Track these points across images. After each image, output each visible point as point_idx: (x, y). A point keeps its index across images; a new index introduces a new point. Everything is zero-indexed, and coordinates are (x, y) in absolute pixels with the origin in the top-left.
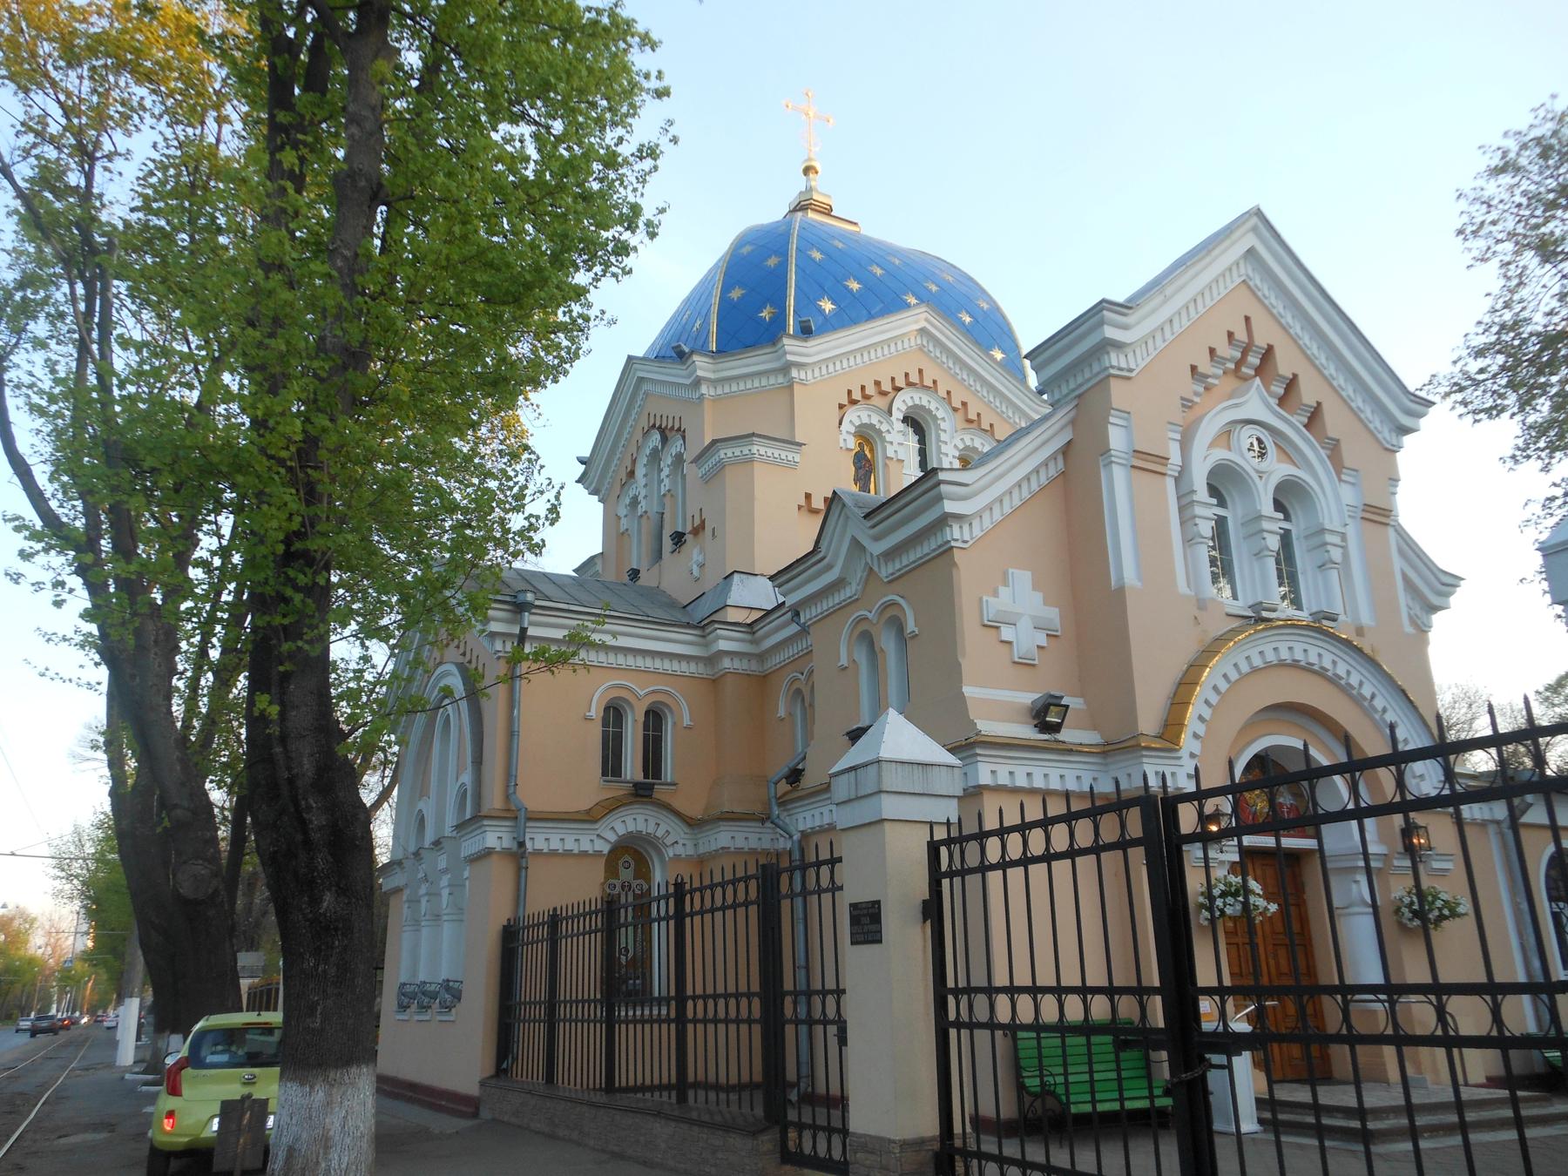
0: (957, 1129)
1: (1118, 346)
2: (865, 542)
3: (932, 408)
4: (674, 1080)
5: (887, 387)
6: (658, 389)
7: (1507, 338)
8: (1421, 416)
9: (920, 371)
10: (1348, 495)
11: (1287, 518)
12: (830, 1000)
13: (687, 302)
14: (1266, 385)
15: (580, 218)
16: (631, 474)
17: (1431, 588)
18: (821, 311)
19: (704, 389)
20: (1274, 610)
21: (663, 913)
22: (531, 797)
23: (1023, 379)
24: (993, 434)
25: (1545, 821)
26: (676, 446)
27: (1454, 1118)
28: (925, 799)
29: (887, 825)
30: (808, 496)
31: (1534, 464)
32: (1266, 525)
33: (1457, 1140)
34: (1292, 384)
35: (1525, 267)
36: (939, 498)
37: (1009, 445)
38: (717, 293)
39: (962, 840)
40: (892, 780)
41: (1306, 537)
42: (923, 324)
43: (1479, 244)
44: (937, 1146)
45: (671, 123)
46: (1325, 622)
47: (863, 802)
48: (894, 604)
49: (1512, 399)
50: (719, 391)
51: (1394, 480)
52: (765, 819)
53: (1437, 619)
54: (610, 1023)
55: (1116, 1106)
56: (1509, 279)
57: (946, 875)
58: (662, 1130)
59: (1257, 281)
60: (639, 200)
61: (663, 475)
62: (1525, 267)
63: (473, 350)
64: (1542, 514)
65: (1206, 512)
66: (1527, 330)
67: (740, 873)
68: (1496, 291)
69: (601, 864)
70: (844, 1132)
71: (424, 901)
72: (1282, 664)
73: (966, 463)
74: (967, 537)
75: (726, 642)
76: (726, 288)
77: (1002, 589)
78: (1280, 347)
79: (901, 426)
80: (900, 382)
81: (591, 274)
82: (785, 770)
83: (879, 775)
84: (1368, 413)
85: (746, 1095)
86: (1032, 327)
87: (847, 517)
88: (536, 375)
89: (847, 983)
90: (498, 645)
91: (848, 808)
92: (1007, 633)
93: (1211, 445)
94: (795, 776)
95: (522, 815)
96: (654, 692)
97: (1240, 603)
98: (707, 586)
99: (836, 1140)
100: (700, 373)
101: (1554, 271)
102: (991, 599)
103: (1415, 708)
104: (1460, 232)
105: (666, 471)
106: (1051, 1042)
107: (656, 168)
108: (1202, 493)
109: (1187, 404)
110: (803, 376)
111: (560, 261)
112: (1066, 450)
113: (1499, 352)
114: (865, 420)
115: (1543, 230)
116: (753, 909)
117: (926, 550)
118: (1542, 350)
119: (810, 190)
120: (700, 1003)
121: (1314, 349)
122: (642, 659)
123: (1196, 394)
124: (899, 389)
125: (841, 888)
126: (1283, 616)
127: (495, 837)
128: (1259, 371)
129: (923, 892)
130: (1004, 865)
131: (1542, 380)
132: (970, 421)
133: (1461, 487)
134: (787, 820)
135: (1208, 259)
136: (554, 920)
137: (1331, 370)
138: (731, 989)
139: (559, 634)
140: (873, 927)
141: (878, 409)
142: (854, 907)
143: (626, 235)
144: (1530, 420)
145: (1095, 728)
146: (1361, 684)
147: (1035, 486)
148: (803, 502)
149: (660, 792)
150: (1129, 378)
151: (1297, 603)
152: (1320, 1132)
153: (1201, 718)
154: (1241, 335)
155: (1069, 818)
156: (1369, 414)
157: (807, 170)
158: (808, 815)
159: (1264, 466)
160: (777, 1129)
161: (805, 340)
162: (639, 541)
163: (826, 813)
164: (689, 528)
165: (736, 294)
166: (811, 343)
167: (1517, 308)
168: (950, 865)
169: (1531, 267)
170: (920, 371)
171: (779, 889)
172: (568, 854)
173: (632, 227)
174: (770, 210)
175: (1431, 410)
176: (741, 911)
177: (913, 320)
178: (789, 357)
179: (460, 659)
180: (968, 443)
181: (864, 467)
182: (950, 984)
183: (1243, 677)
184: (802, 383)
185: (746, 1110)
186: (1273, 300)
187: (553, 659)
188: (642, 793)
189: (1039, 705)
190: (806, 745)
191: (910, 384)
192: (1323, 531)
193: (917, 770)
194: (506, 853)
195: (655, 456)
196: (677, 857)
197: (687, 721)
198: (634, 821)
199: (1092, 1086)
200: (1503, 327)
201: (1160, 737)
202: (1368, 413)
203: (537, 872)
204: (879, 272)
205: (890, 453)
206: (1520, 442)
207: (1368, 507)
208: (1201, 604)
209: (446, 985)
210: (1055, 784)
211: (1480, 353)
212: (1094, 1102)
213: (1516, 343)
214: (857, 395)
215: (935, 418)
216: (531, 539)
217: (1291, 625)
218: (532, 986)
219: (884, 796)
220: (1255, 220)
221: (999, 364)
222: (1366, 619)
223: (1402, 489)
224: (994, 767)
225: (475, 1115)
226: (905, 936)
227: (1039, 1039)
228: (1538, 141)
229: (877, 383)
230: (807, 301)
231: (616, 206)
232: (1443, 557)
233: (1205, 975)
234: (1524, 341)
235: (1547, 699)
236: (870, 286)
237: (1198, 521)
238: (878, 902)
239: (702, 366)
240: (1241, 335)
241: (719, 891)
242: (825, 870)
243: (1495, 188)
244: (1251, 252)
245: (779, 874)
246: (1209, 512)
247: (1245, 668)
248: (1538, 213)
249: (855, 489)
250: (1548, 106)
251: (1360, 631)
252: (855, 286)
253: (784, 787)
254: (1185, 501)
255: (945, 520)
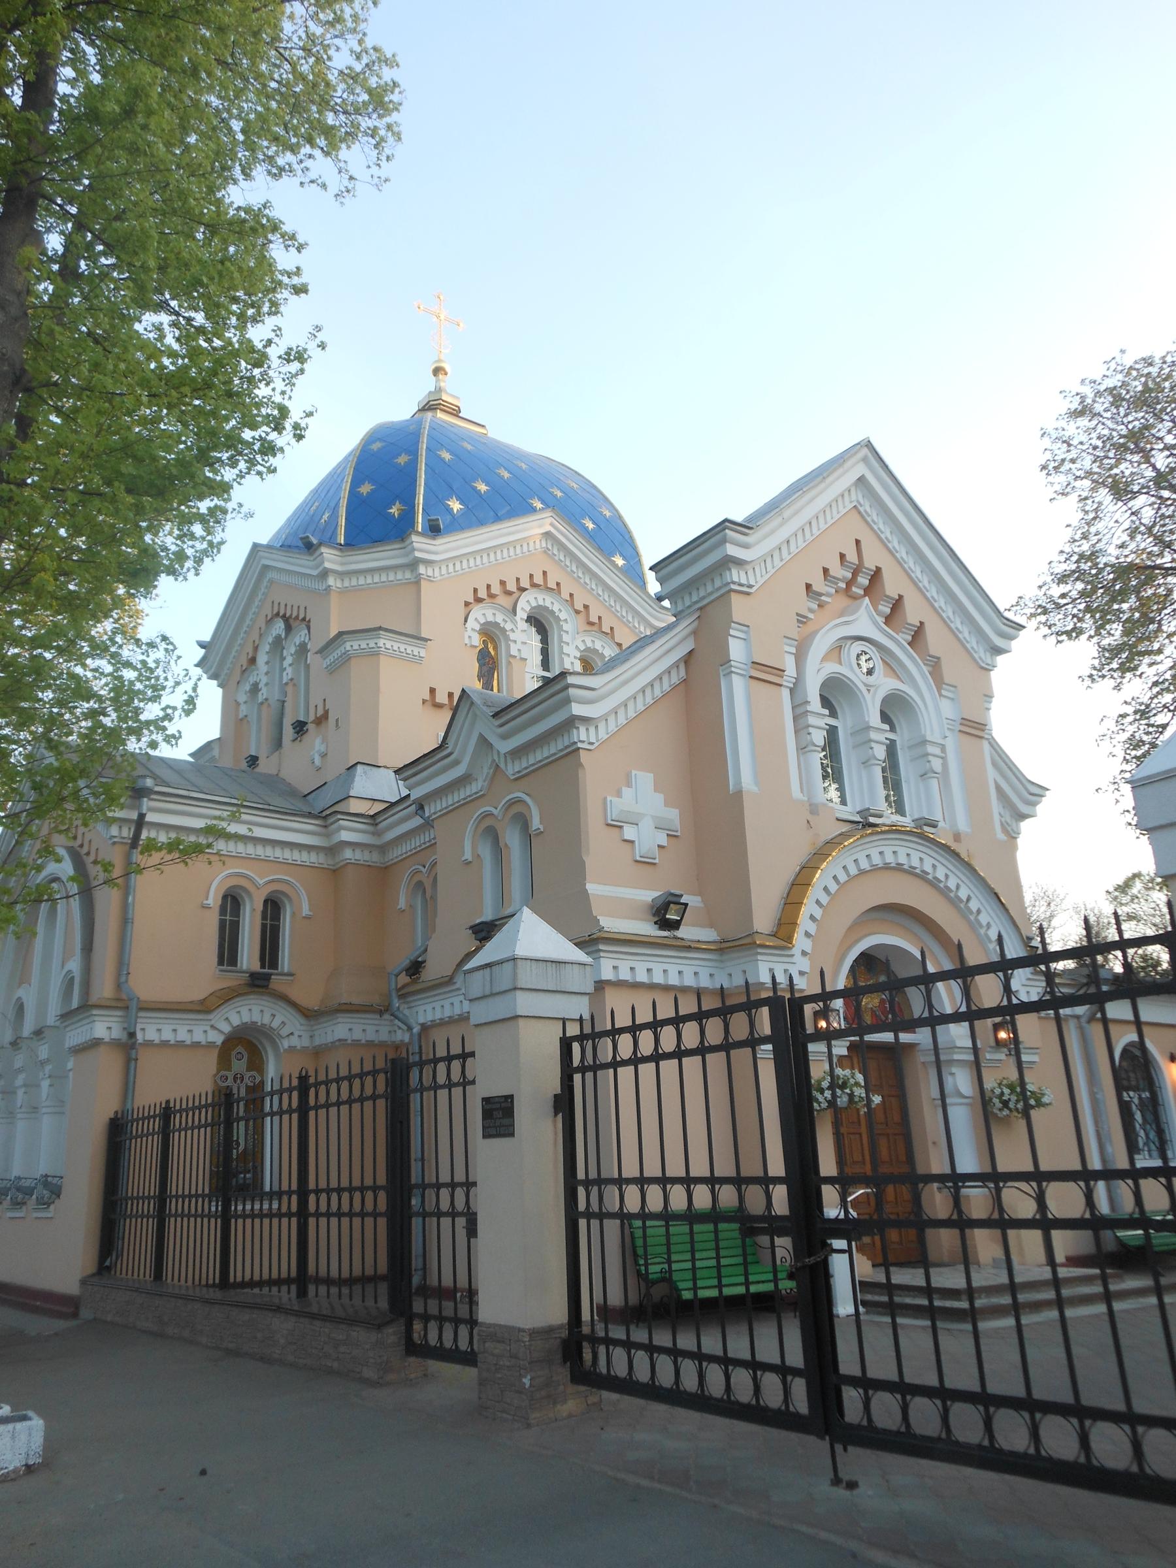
0: (586, 1315)
1: (740, 563)
2: (492, 739)
3: (555, 609)
4: (294, 1274)
5: (512, 586)
6: (284, 578)
7: (1085, 566)
8: (1012, 638)
9: (545, 573)
10: (947, 709)
11: (893, 729)
12: (460, 1193)
13: (315, 492)
14: (875, 605)
15: (220, 409)
16: (253, 661)
17: (1020, 797)
18: (449, 510)
19: (331, 581)
20: (880, 816)
21: (275, 1108)
22: (143, 987)
23: (643, 585)
24: (613, 638)
25: (1131, 1017)
26: (300, 636)
27: (1021, 1298)
28: (558, 996)
29: (521, 1022)
30: (432, 691)
31: (1109, 683)
32: (873, 735)
33: (1010, 1322)
34: (897, 604)
35: (1100, 503)
36: (567, 701)
37: (634, 653)
38: (346, 486)
39: (595, 1036)
40: (527, 976)
41: (910, 748)
42: (548, 528)
43: (1060, 479)
44: (565, 1334)
45: (318, 329)
46: (926, 828)
47: (498, 999)
48: (520, 801)
49: (1088, 623)
50: (346, 584)
51: (989, 696)
52: (384, 1010)
53: (1025, 825)
54: (226, 1218)
55: (741, 1290)
56: (1087, 512)
57: (577, 1070)
58: (282, 1326)
59: (866, 507)
60: (287, 403)
61: (286, 663)
62: (1100, 503)
63: (113, 540)
64: (1116, 729)
65: (819, 721)
66: (1102, 561)
67: (368, 1067)
68: (1075, 523)
69: (215, 1054)
70: (472, 1322)
71: (20, 1092)
72: (887, 867)
73: (588, 667)
74: (593, 740)
75: (349, 833)
76: (356, 483)
77: (624, 789)
78: (882, 563)
79: (525, 626)
80: (525, 583)
81: (236, 471)
82: (406, 963)
83: (515, 975)
84: (965, 633)
85: (357, 1289)
86: (658, 537)
87: (475, 715)
88: (176, 566)
89: (480, 1173)
90: (114, 831)
91: (482, 1004)
92: (629, 832)
93: (825, 659)
94: (415, 968)
95: (134, 1005)
96: (273, 881)
97: (849, 808)
98: (329, 775)
99: (463, 1331)
100: (327, 565)
101: (1125, 508)
102: (615, 800)
103: (1007, 910)
104: (1044, 467)
105: (289, 660)
106: (679, 1230)
107: (302, 371)
108: (815, 704)
109: (802, 620)
110: (430, 573)
111: (204, 458)
112: (688, 659)
113: (1077, 579)
114: (490, 618)
115: (1115, 471)
116: (381, 1103)
117: (553, 751)
118: (1115, 580)
119: (439, 390)
120: (323, 1196)
121: (917, 573)
122: (268, 848)
123: (811, 610)
124: (524, 590)
125: (473, 1082)
126: (888, 822)
127: (104, 1027)
128: (868, 591)
129: (554, 1085)
130: (636, 1061)
131: (1116, 607)
132: (591, 624)
133: (1056, 711)
134: (406, 1012)
135: (822, 486)
136: (167, 1113)
137: (933, 592)
138: (334, 1184)
139: (200, 824)
140: (506, 1121)
141: (502, 608)
142: (486, 1100)
143: (273, 436)
144: (1105, 642)
145: (711, 925)
146: (958, 887)
147: (658, 692)
148: (427, 697)
149: (277, 982)
150: (748, 594)
151: (900, 811)
152: (932, 1313)
153: (812, 918)
154: (852, 557)
155: (700, 1016)
156: (966, 634)
157: (437, 371)
158: (429, 1007)
159: (871, 680)
160: (402, 1321)
161: (434, 538)
162: (259, 730)
163: (438, 1009)
164: (312, 718)
165: (365, 489)
166: (439, 541)
167: (1094, 539)
168: (582, 1060)
169: (1105, 503)
170: (545, 573)
171: (400, 1082)
172: (180, 1045)
173: (279, 428)
174: (400, 409)
175: (1022, 633)
176: (368, 1105)
177: (535, 528)
178: (418, 554)
179: (71, 843)
180: (589, 644)
181: (488, 664)
182: (581, 1175)
183: (852, 879)
184: (429, 579)
185: (370, 1303)
186: (881, 526)
187: (186, 849)
188: (258, 983)
189: (660, 902)
190: (427, 938)
191: (534, 585)
192: (924, 742)
193: (551, 968)
194: (116, 1044)
195: (278, 644)
196: (292, 1049)
197: (306, 910)
198: (250, 1011)
199: (719, 1272)
200: (1082, 556)
201: (774, 935)
202: (965, 633)
203: (147, 1062)
204: (506, 475)
205: (514, 652)
206: (1096, 663)
207: (965, 721)
208: (814, 809)
209: (45, 1181)
210: (689, 981)
211: (1062, 579)
212: (720, 1286)
213: (1094, 572)
214: (482, 594)
215: (558, 619)
216: (164, 729)
217: (894, 830)
218: (141, 1178)
219: (519, 993)
220: (865, 451)
221: (620, 569)
222: (963, 825)
223: (995, 705)
224: (616, 963)
225: (75, 1315)
226: (536, 1129)
227: (667, 1227)
228: (1110, 390)
229: (503, 583)
230: (436, 500)
231: (258, 405)
232: (1032, 773)
233: (828, 1165)
234: (1101, 571)
235: (1116, 898)
236: (498, 488)
237: (811, 730)
238: (512, 1097)
239: (330, 558)
240: (852, 557)
241: (334, 1086)
242: (456, 1065)
243: (1077, 430)
244: (861, 480)
245: (409, 1067)
246: (821, 722)
247: (853, 871)
248: (1111, 454)
249: (478, 686)
250: (1118, 360)
251: (957, 837)
252: (483, 487)
253: (404, 979)
254: (800, 710)
255: (572, 722)
